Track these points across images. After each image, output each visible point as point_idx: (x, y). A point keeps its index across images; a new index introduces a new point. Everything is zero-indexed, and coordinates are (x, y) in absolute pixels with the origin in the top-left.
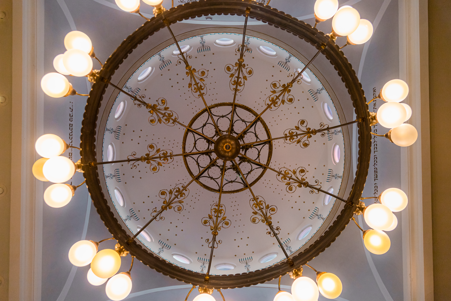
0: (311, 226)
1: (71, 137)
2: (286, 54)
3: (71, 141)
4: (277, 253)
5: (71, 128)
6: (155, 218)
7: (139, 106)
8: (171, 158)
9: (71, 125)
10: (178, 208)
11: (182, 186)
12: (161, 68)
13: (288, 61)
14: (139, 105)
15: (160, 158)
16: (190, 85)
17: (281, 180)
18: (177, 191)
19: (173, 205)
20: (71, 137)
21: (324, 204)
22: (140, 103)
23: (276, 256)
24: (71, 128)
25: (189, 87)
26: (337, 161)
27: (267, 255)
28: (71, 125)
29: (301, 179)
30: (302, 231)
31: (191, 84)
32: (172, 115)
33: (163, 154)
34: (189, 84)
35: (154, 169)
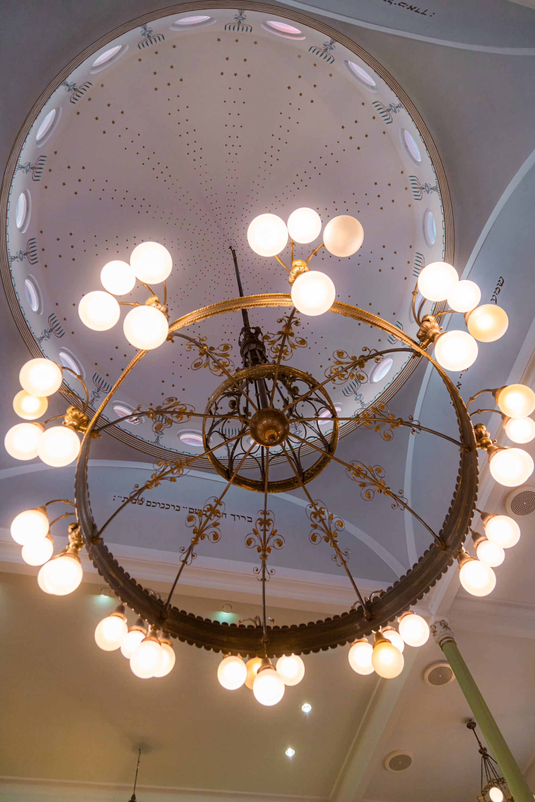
0: (403, 130)
1: (166, 506)
2: (61, 91)
3: (172, 508)
4: (427, 211)
5: (153, 504)
6: (345, 562)
7: (194, 556)
8: (268, 514)
9: (149, 504)
10: (339, 525)
11: (310, 507)
12: (34, 262)
13: (74, 88)
14: (193, 556)
15: (265, 530)
16: (173, 479)
17: (342, 382)
18: (315, 517)
19: (333, 530)
20: (166, 506)
21: (372, 87)
22: (190, 556)
23: (430, 213)
24: (153, 504)
25: (175, 481)
26: (297, 31)
27: (424, 227)
28: (149, 504)
29: (352, 361)
30: (406, 147)
31: (172, 478)
32: (210, 505)
33: (261, 525)
34: (171, 480)
35: (280, 544)
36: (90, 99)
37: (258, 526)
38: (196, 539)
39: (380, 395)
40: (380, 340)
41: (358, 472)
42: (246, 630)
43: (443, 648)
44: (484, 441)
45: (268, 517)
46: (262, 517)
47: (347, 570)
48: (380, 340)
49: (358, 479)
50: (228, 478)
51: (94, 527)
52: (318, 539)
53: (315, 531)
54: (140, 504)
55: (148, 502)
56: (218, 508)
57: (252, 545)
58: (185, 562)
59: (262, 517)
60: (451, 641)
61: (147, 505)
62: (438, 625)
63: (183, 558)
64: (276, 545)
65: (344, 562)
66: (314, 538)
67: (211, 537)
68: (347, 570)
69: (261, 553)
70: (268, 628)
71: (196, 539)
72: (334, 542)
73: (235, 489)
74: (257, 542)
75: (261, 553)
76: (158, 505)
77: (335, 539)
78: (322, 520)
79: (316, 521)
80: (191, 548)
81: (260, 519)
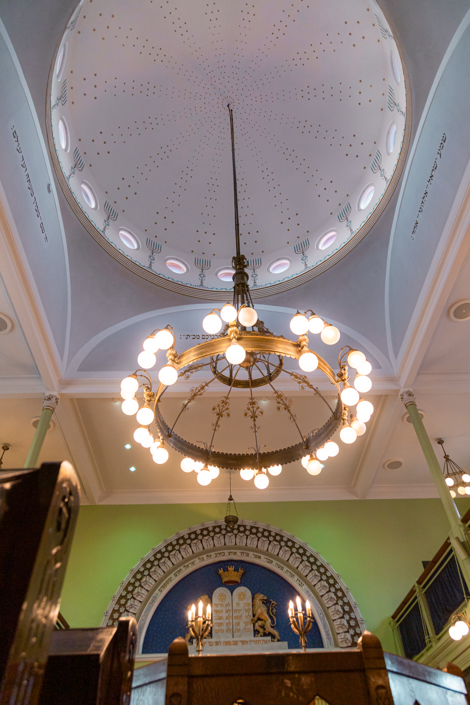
14: (218, 426)
28: (204, 337)
36: (85, 153)
37: (249, 405)
38: (219, 418)
39: (364, 223)
40: (365, 168)
41: (296, 377)
42: (250, 456)
43: (408, 408)
44: (343, 378)
45: (253, 401)
46: (251, 401)
47: (296, 424)
48: (365, 168)
49: (297, 380)
50: (229, 384)
51: (168, 429)
52: (281, 409)
53: (279, 405)
54: (198, 338)
55: (203, 335)
56: (227, 401)
57: (248, 415)
58: (215, 430)
59: (251, 401)
60: (413, 404)
61: (203, 338)
62: (405, 394)
63: (214, 428)
64: (260, 414)
65: (295, 420)
66: (279, 409)
67: (226, 415)
68: (296, 424)
69: (253, 419)
70: (260, 454)
71: (219, 418)
72: (289, 410)
73: (234, 389)
74: (250, 414)
75: (253, 419)
76: (210, 337)
77: (289, 409)
78: (282, 400)
79: (279, 400)
80: (217, 423)
81: (250, 402)
